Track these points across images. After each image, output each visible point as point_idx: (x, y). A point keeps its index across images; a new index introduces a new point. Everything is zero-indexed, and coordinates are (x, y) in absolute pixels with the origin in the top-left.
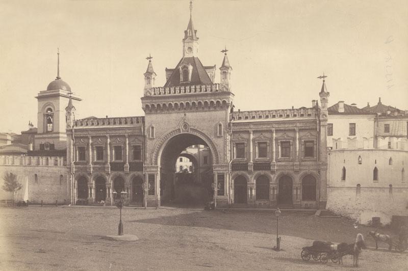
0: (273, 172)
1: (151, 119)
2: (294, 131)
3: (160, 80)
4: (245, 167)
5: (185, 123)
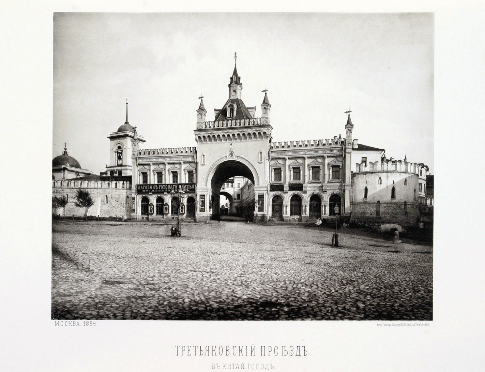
0: (305, 192)
1: (203, 148)
2: (284, 159)
3: (210, 116)
4: (280, 188)
5: (231, 151)
